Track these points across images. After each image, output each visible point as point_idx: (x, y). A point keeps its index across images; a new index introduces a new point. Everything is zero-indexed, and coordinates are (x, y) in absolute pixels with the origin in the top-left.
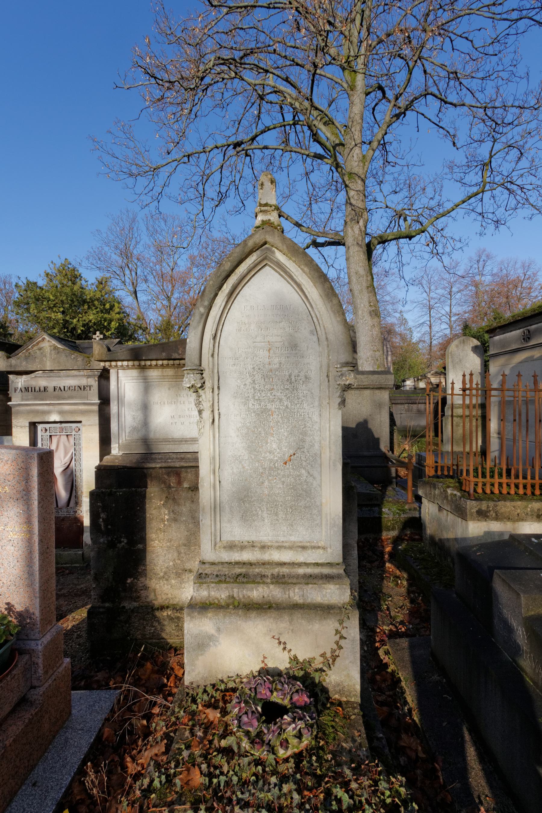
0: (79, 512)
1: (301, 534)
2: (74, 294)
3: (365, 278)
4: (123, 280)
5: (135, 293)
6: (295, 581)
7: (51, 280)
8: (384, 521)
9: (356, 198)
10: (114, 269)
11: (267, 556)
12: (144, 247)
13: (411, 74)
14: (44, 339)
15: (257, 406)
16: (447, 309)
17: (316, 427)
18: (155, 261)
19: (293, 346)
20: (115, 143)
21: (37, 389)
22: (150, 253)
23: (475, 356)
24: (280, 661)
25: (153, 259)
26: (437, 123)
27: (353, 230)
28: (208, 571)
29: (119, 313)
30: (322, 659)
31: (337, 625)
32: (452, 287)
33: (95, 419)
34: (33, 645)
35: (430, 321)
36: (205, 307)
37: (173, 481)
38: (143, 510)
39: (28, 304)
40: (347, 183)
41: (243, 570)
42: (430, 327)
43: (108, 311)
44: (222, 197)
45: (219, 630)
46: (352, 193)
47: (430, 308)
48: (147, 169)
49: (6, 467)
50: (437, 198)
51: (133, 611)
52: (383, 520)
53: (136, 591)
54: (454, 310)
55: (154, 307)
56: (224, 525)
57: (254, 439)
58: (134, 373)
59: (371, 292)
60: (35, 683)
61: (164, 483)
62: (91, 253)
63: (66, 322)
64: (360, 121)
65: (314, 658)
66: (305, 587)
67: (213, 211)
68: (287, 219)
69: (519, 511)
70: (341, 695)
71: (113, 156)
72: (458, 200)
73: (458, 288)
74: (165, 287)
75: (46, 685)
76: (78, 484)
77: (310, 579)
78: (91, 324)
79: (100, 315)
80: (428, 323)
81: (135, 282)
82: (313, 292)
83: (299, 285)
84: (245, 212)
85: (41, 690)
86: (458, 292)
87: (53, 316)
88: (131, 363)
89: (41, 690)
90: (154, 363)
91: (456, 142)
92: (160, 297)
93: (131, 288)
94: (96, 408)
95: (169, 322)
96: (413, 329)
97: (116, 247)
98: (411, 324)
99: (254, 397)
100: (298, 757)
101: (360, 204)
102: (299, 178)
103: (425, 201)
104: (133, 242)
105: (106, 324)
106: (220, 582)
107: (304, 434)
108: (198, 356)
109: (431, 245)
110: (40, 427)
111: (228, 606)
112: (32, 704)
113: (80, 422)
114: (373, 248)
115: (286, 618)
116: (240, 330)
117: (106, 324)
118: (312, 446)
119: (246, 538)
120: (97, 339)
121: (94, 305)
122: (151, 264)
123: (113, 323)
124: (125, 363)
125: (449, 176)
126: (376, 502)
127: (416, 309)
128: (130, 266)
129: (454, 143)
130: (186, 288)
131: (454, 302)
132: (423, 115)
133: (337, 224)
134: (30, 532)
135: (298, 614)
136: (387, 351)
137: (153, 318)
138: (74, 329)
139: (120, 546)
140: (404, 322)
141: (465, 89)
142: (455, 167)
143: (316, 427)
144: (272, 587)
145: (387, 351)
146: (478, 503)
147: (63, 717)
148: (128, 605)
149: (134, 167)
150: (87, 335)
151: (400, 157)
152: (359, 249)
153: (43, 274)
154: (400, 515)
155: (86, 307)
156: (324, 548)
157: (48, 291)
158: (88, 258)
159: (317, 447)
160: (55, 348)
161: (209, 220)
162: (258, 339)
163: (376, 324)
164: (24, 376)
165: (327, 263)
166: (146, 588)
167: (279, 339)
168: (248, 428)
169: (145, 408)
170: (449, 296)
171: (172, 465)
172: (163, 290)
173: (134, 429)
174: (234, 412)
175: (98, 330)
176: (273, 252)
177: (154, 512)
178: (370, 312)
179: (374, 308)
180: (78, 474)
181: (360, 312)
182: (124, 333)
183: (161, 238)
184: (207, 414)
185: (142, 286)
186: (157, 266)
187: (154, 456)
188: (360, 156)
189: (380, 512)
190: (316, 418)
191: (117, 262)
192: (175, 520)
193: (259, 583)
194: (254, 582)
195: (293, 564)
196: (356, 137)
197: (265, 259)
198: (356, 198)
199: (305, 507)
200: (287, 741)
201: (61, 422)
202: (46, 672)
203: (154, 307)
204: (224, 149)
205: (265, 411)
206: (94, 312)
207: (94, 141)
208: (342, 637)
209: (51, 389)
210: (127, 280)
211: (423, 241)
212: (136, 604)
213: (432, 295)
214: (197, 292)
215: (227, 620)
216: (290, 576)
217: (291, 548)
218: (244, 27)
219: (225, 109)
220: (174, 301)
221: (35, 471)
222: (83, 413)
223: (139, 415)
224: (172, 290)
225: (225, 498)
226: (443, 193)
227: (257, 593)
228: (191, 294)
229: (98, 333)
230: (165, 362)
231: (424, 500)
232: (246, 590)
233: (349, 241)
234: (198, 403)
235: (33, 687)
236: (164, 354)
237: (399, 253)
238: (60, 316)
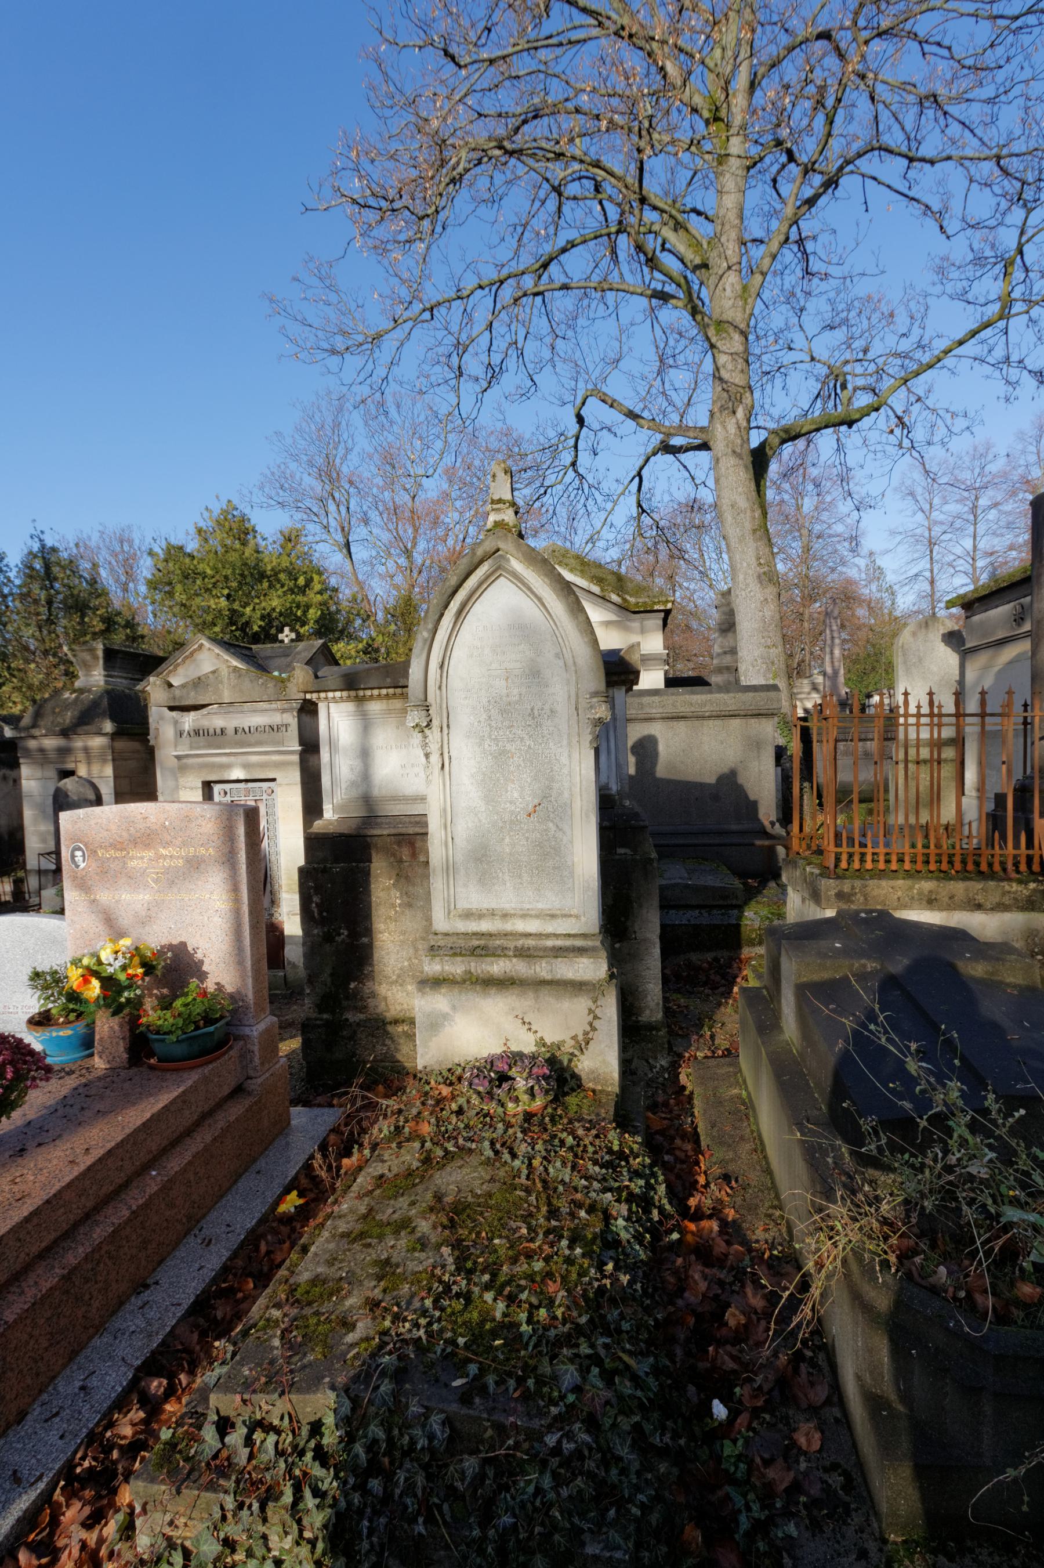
0: (276, 915)
1: (550, 901)
2: (245, 564)
3: (749, 513)
4: (325, 522)
5: (348, 545)
6: (541, 954)
7: (206, 540)
8: (745, 932)
9: (730, 366)
10: (308, 502)
11: (509, 926)
12: (359, 460)
13: (831, 123)
14: (201, 646)
15: (494, 748)
16: (968, 544)
17: (565, 771)
18: (381, 483)
19: (534, 674)
20: (305, 298)
21: (211, 732)
22: (372, 468)
23: (949, 650)
24: (526, 1043)
25: (379, 481)
26: (906, 191)
27: (725, 427)
28: (441, 943)
29: (320, 593)
30: (573, 1042)
31: (590, 1003)
32: (977, 499)
33: (295, 776)
34: (247, 1031)
35: (932, 571)
36: (428, 631)
37: (405, 853)
38: (367, 892)
39: (170, 583)
40: (714, 340)
41: (482, 942)
42: (932, 582)
43: (302, 590)
44: (494, 373)
45: (454, 1008)
46: (722, 359)
47: (931, 544)
48: (360, 338)
49: (209, 825)
50: (916, 332)
51: (358, 1024)
52: (743, 929)
53: (362, 999)
54: (982, 545)
55: (382, 569)
56: (458, 889)
57: (491, 787)
58: (350, 707)
59: (760, 539)
60: (251, 1073)
61: (394, 855)
62: (266, 476)
63: (233, 612)
64: (737, 221)
65: (564, 1042)
66: (554, 960)
67: (479, 401)
68: (611, 406)
69: (900, 893)
70: (596, 1084)
71: (304, 323)
72: (959, 335)
73: (990, 498)
74: (401, 532)
75: (264, 1077)
76: (274, 873)
77: (559, 952)
78: (274, 615)
79: (290, 597)
80: (928, 574)
81: (346, 525)
82: (557, 606)
83: (540, 599)
84: (539, 394)
85: (259, 1081)
86: (990, 507)
87: (212, 603)
88: (345, 694)
89: (259, 1081)
90: (376, 692)
91: (944, 224)
92: (392, 551)
93: (340, 538)
94: (296, 758)
95: (410, 599)
96: (895, 587)
97: (311, 464)
98: (890, 578)
99: (490, 736)
100: (528, 1116)
101: (738, 379)
102: (640, 317)
103: (891, 341)
104: (341, 451)
105: (299, 613)
106: (455, 955)
107: (552, 779)
108: (422, 689)
109: (898, 431)
110: (217, 788)
111: (464, 981)
112: (249, 1094)
113: (274, 780)
114: (770, 453)
115: (531, 994)
116: (471, 656)
117: (299, 613)
118: (561, 794)
119: (485, 906)
120: (286, 640)
121: (279, 581)
122: (375, 490)
123: (311, 611)
124: (338, 694)
125: (938, 289)
126: (734, 902)
127: (900, 548)
128: (337, 495)
129: (941, 227)
130: (441, 532)
131: (981, 528)
132: (875, 179)
133: (699, 416)
134: (237, 901)
135: (545, 990)
136: (833, 638)
137: (382, 593)
138: (247, 624)
139: (339, 939)
140: (877, 573)
141: (956, 123)
142: (953, 269)
143: (565, 771)
144: (514, 960)
145: (833, 638)
146: (838, 882)
147: (282, 1126)
148: (352, 1017)
149: (339, 338)
150: (268, 635)
151: (835, 260)
152: (737, 461)
153: (192, 530)
154: (771, 921)
155: (266, 584)
156: (577, 917)
157: (202, 560)
158: (261, 488)
159: (566, 795)
160: (235, 669)
161: (473, 417)
162: (494, 666)
163: (770, 598)
164: (192, 713)
165: (693, 479)
166: (373, 995)
167: (518, 665)
168: (484, 774)
169: (365, 754)
170: (972, 517)
171: (403, 831)
172: (398, 538)
173: (353, 784)
174: (466, 754)
175: (287, 625)
176: (508, 560)
177: (381, 894)
178: (759, 577)
179: (766, 569)
180: (273, 858)
181: (741, 577)
182: (330, 627)
183: (391, 438)
184: (435, 758)
185: (358, 533)
186: (386, 493)
187: (379, 820)
188: (738, 287)
189: (740, 917)
190: (564, 760)
191: (312, 489)
192: (410, 905)
193: (499, 956)
194: (494, 955)
195: (540, 936)
196: (729, 253)
197: (499, 568)
198: (730, 366)
199: (554, 868)
200: (517, 1097)
201: (247, 781)
202: (262, 1064)
203: (382, 569)
204: (494, 288)
205: (503, 752)
206: (280, 592)
207: (271, 301)
208: (596, 1017)
209: (230, 731)
210: (333, 523)
211: (882, 423)
212: (362, 1016)
213: (935, 515)
214: (461, 537)
215: (463, 997)
216: (536, 948)
217: (537, 916)
218: (521, 73)
219: (496, 205)
220: (419, 559)
221: (241, 831)
222: (278, 765)
223: (357, 764)
224: (415, 538)
225: (459, 858)
226: (928, 322)
227: (497, 967)
228: (450, 542)
229: (287, 629)
230: (391, 691)
231: (790, 890)
232: (483, 963)
233: (719, 445)
234: (425, 745)
235: (249, 1078)
236: (389, 680)
237: (840, 448)
238: (223, 602)
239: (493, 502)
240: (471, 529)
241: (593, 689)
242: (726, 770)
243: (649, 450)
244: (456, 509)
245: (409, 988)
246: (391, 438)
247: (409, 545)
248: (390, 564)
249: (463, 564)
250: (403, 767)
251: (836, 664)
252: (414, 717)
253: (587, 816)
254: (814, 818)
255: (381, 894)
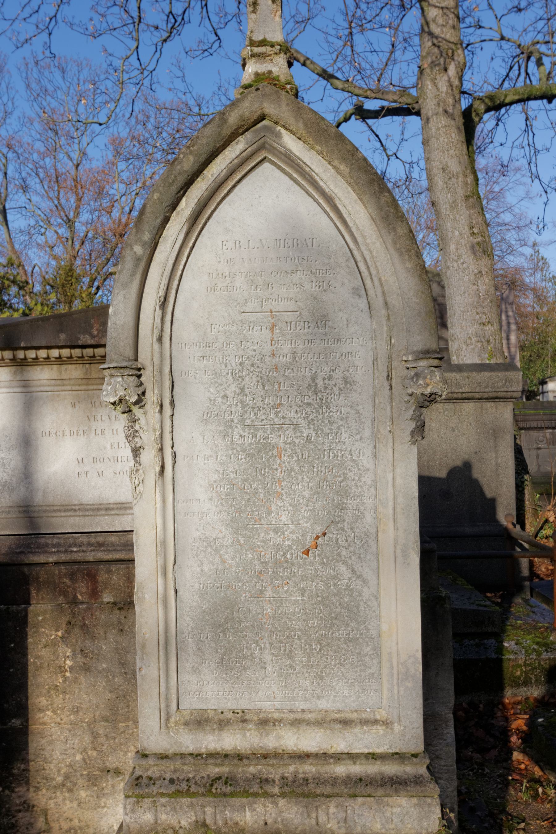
1: (339, 696)
3: (461, 179)
6: (328, 790)
8: (508, 668)
9: (440, 21)
11: (271, 741)
15: (249, 440)
17: (368, 479)
18: (43, 149)
19: (320, 320)
22: (33, 133)
25: (39, 146)
27: (435, 85)
28: (154, 772)
38: (22, 650)
41: (225, 770)
52: (505, 665)
55: (41, 240)
57: (244, 505)
59: (473, 207)
61: (64, 593)
66: (350, 802)
67: (158, 50)
68: (304, 64)
74: (63, 201)
83: (329, 199)
84: (221, 51)
90: (43, 354)
92: (52, 220)
95: (71, 270)
99: (242, 421)
101: (449, 35)
106: (178, 793)
107: (344, 493)
108: (131, 341)
116: (214, 289)
118: (360, 517)
119: (230, 705)
122: (35, 156)
130: (106, 203)
133: (403, 73)
136: (509, 324)
143: (368, 479)
144: (282, 802)
145: (509, 324)
154: (539, 654)
156: (386, 723)
159: (369, 518)
161: (150, 68)
162: (250, 306)
163: (484, 270)
165: (385, 150)
166: (28, 807)
171: (79, 557)
174: (202, 450)
176: (279, 135)
177: (44, 652)
178: (472, 247)
179: (480, 239)
181: (453, 247)
183: (54, 104)
184: (149, 456)
186: (47, 160)
187: (42, 541)
189: (500, 650)
190: (366, 461)
192: (86, 669)
193: (256, 795)
194: (246, 794)
195: (324, 757)
198: (440, 21)
199: (348, 641)
203: (41, 240)
205: (265, 447)
214: (127, 209)
216: (319, 781)
217: (319, 723)
220: (80, 228)
224: (78, 207)
225: (187, 623)
228: (116, 214)
230: (66, 352)
233: (429, 106)
234: (132, 434)
236: (63, 336)
239: (252, 43)
240: (137, 201)
241: (419, 347)
242: (459, 463)
243: (341, 116)
244: (122, 182)
245: (83, 794)
246: (54, 104)
247: (71, 215)
248: (50, 234)
249: (208, 137)
250: (81, 461)
251: (513, 350)
252: (115, 387)
253: (405, 556)
254: (535, 514)
255: (44, 652)
